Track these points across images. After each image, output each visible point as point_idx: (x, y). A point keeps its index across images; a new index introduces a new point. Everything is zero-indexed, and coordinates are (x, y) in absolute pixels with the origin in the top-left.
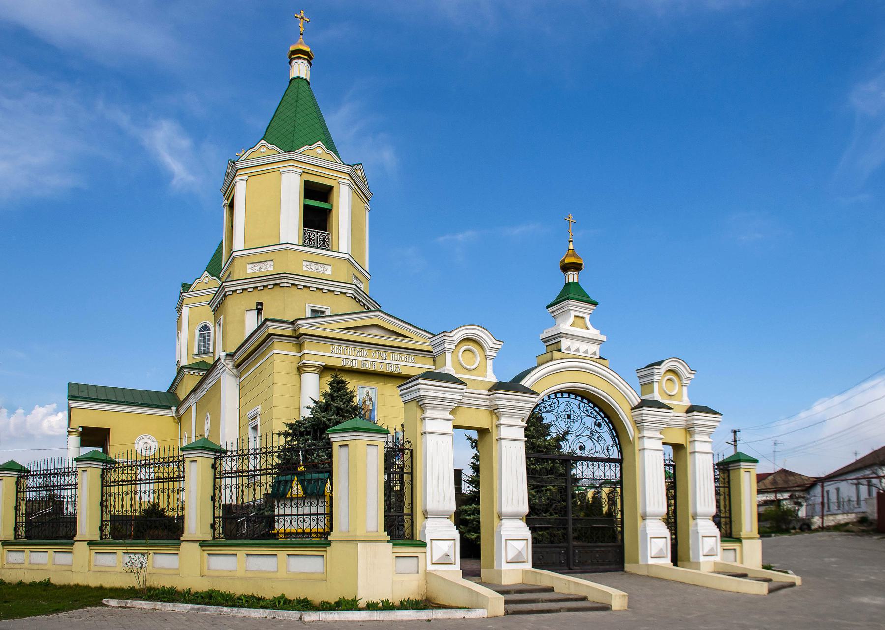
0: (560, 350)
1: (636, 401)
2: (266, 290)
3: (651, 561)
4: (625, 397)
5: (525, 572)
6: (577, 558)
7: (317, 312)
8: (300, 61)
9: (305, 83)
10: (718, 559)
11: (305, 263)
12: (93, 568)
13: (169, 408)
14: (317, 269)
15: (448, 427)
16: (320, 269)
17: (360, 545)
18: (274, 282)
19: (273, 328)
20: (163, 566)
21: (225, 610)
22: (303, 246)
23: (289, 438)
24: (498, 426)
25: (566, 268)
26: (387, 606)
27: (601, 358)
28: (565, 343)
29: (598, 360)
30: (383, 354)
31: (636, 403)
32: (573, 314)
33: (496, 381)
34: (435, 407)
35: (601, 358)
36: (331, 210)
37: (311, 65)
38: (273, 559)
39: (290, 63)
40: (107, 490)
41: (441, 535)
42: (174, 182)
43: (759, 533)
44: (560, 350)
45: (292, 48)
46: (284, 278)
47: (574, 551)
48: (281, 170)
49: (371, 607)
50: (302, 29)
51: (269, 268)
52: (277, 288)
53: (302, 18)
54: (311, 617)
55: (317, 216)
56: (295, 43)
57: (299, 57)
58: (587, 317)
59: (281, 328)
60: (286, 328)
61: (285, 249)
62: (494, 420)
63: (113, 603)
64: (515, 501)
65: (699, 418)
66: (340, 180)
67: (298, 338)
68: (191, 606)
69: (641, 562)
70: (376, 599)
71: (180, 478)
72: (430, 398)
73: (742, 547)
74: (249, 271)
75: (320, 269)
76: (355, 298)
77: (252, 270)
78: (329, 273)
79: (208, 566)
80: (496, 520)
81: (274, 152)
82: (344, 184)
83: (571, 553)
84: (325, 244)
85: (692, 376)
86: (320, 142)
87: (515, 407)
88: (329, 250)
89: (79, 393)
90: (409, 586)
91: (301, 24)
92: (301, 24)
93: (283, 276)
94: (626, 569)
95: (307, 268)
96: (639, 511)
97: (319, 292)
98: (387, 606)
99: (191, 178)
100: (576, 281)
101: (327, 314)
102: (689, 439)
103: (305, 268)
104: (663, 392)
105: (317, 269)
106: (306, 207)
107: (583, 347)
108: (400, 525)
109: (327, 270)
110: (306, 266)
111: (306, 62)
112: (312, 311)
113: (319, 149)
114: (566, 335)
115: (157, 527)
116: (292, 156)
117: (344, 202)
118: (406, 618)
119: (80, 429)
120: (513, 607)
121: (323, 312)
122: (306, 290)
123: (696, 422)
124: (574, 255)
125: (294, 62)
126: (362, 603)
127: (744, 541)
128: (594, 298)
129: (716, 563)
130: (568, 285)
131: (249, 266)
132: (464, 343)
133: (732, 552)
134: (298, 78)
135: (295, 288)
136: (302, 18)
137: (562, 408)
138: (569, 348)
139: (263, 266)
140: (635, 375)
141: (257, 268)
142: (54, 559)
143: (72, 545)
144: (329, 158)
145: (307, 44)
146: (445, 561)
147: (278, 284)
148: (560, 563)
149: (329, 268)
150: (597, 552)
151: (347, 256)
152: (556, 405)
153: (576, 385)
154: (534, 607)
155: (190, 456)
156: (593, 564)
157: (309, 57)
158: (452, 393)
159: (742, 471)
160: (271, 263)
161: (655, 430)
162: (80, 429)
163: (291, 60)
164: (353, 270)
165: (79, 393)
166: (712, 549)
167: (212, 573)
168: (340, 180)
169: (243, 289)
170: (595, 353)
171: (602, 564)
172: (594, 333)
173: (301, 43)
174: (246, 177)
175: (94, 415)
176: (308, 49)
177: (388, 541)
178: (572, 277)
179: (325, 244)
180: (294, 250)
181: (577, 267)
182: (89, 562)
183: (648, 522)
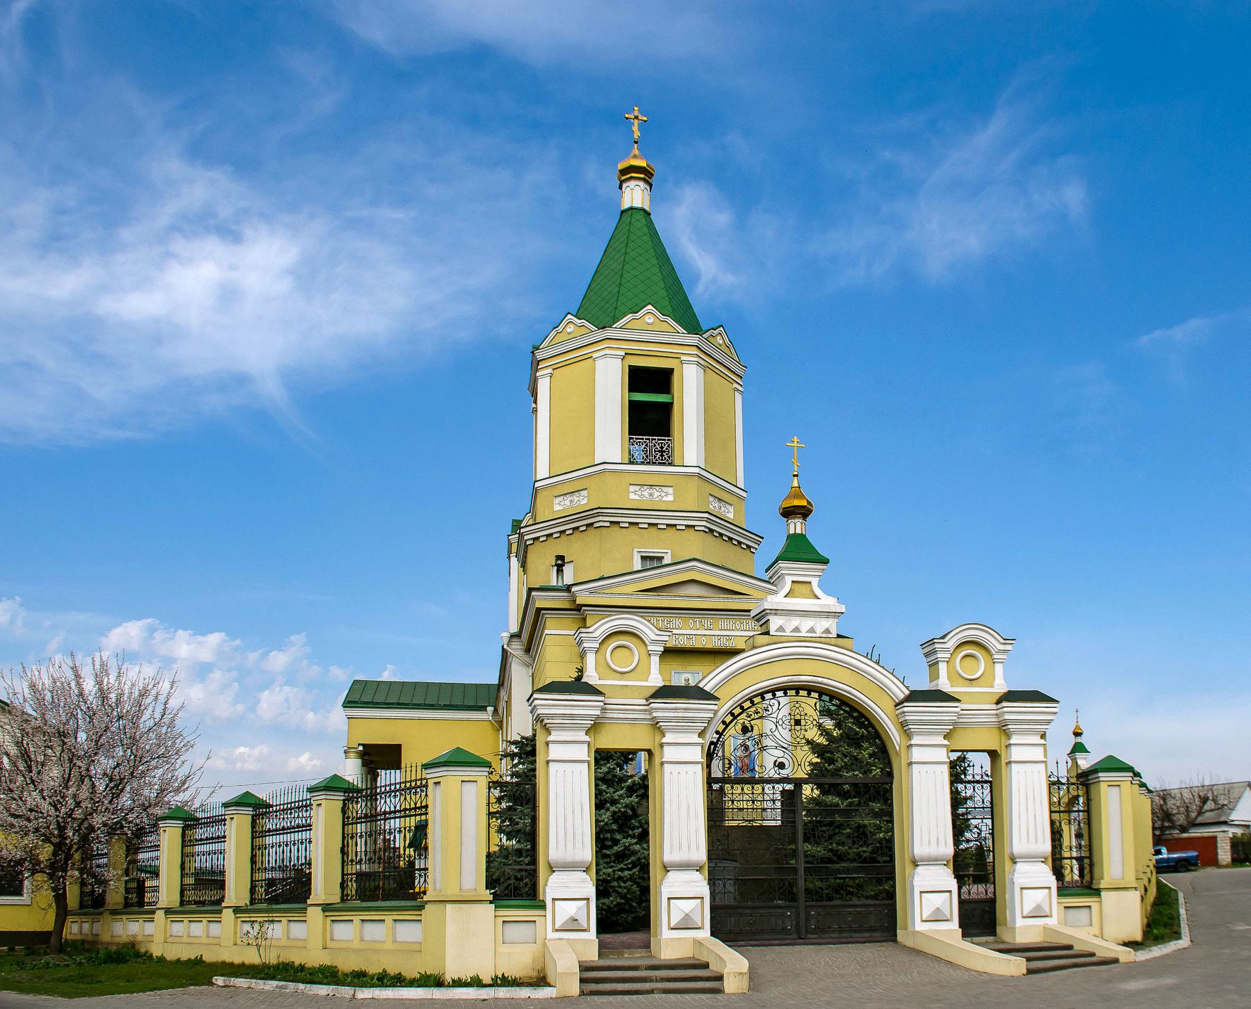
0: (767, 633)
1: (901, 693)
2: (577, 534)
3: (920, 927)
4: (882, 688)
5: (698, 943)
6: (813, 921)
7: (652, 558)
8: (632, 183)
9: (640, 216)
10: (1052, 922)
11: (632, 488)
12: (329, 944)
13: (483, 708)
14: (651, 495)
15: (583, 753)
16: (656, 494)
17: (449, 906)
18: (585, 523)
19: (541, 600)
20: (302, 936)
21: (301, 986)
22: (631, 463)
23: (516, 761)
24: (662, 745)
25: (788, 513)
26: (476, 982)
27: (839, 636)
28: (775, 623)
29: (833, 641)
30: (707, 623)
31: (902, 696)
32: (789, 580)
33: (661, 684)
34: (562, 727)
35: (839, 636)
36: (672, 404)
37: (651, 186)
38: (380, 925)
39: (620, 188)
40: (258, 841)
41: (570, 892)
42: (700, 288)
43: (490, 884)
44: (767, 633)
45: (621, 166)
46: (598, 515)
47: (808, 914)
48: (595, 355)
49: (458, 983)
50: (637, 134)
51: (582, 501)
52: (591, 530)
53: (636, 117)
54: (365, 994)
55: (650, 417)
56: (626, 155)
57: (632, 178)
58: (815, 581)
59: (553, 598)
60: (558, 598)
61: (603, 471)
62: (657, 738)
63: (219, 981)
64: (685, 844)
65: (1013, 711)
66: (683, 358)
67: (579, 610)
68: (275, 983)
69: (910, 929)
70: (466, 975)
71: (308, 827)
72: (554, 716)
73: (1100, 902)
74: (557, 508)
75: (656, 494)
76: (711, 531)
77: (560, 506)
78: (670, 498)
79: (332, 934)
80: (1008, 863)
81: (584, 331)
82: (689, 362)
83: (802, 915)
84: (664, 457)
85: (1008, 647)
86: (650, 307)
87: (684, 719)
88: (670, 464)
89: (363, 696)
90: (517, 961)
91: (635, 128)
92: (635, 128)
93: (597, 511)
94: (899, 938)
95: (635, 496)
96: (1007, 852)
97: (653, 529)
98: (476, 982)
99: (729, 279)
100: (799, 531)
101: (665, 562)
102: (1004, 742)
103: (632, 496)
104: (954, 676)
105: (651, 495)
106: (633, 406)
107: (806, 624)
108: (514, 879)
109: (667, 494)
110: (635, 492)
111: (642, 184)
112: (643, 558)
113: (649, 316)
114: (776, 612)
115: (286, 891)
116: (609, 333)
117: (690, 389)
118: (464, 997)
119: (361, 748)
120: (593, 987)
121: (660, 559)
122: (633, 528)
123: (1007, 717)
124: (800, 496)
125: (624, 186)
126: (448, 978)
127: (1102, 893)
128: (823, 552)
129: (1046, 929)
130: (791, 537)
131: (557, 500)
132: (609, 642)
133: (1087, 910)
134: (631, 208)
135: (616, 528)
136: (636, 117)
137: (785, 711)
138: (781, 629)
139: (575, 498)
140: (921, 652)
141: (567, 502)
142: (208, 931)
143: (220, 912)
144: (665, 327)
145: (642, 156)
146: (573, 926)
147: (592, 524)
148: (784, 931)
149: (670, 490)
150: (850, 913)
151: (697, 470)
152: (775, 708)
153: (795, 678)
154: (647, 986)
155: (321, 796)
156: (841, 930)
157: (646, 174)
158: (587, 707)
159: (1103, 786)
160: (585, 493)
161: (938, 734)
162: (361, 748)
163: (622, 183)
164: (709, 489)
165: (363, 696)
166: (1038, 907)
167: (334, 945)
168: (683, 358)
169: (587, 525)
170: (827, 631)
171: (856, 931)
172: (828, 602)
173: (635, 157)
174: (549, 371)
175: (382, 727)
176: (643, 164)
177: (491, 902)
178: (796, 526)
179: (664, 457)
180: (622, 471)
181: (804, 512)
182: (235, 933)
183: (1020, 867)
